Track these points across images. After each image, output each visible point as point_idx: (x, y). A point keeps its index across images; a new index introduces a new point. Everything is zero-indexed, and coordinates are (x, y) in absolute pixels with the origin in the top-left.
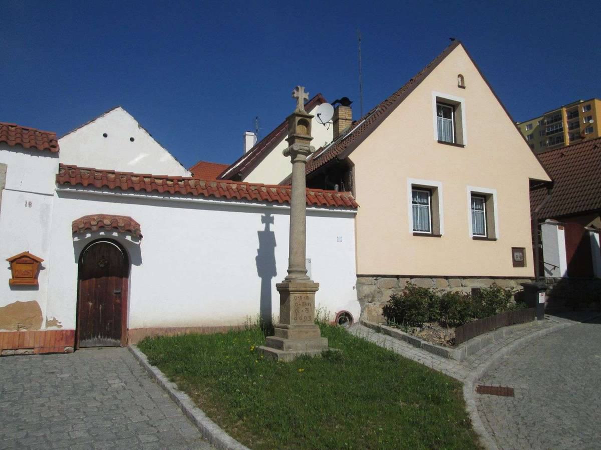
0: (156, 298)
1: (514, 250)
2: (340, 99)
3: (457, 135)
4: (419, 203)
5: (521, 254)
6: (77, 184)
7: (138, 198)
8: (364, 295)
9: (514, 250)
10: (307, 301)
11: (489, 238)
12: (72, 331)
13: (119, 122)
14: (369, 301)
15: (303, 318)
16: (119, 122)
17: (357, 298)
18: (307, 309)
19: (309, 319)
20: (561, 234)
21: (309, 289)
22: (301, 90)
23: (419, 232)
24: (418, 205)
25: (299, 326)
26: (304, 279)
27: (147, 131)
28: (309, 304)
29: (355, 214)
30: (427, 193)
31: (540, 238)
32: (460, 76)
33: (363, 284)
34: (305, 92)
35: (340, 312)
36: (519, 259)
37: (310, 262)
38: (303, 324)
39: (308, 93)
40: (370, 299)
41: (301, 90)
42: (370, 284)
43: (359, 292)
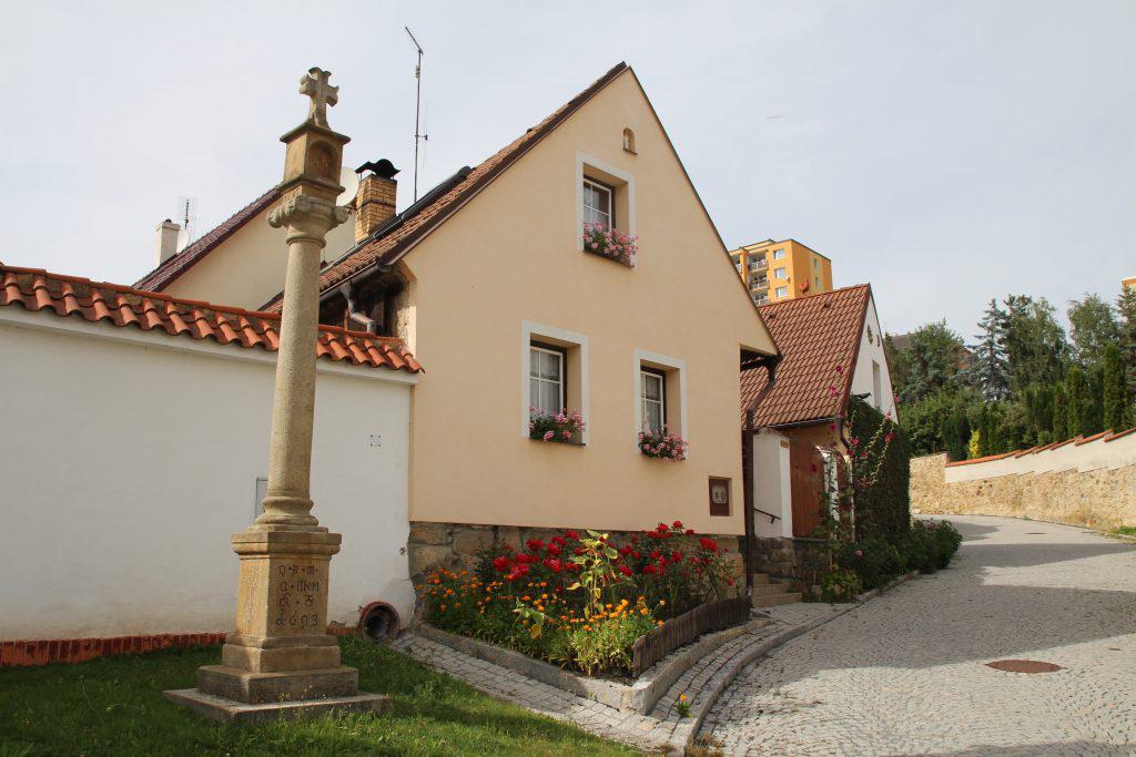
1: (714, 482)
2: (374, 161)
3: (690, 189)
5: (724, 489)
8: (424, 568)
9: (714, 482)
10: (310, 579)
12: (739, 537)
17: (406, 575)
18: (309, 599)
19: (311, 622)
20: (784, 455)
25: (290, 640)
26: (306, 524)
30: (558, 357)
31: (745, 471)
32: (628, 132)
33: (423, 542)
35: (369, 606)
36: (718, 500)
37: (530, 130)
38: (299, 635)
42: (438, 541)
43: (412, 559)
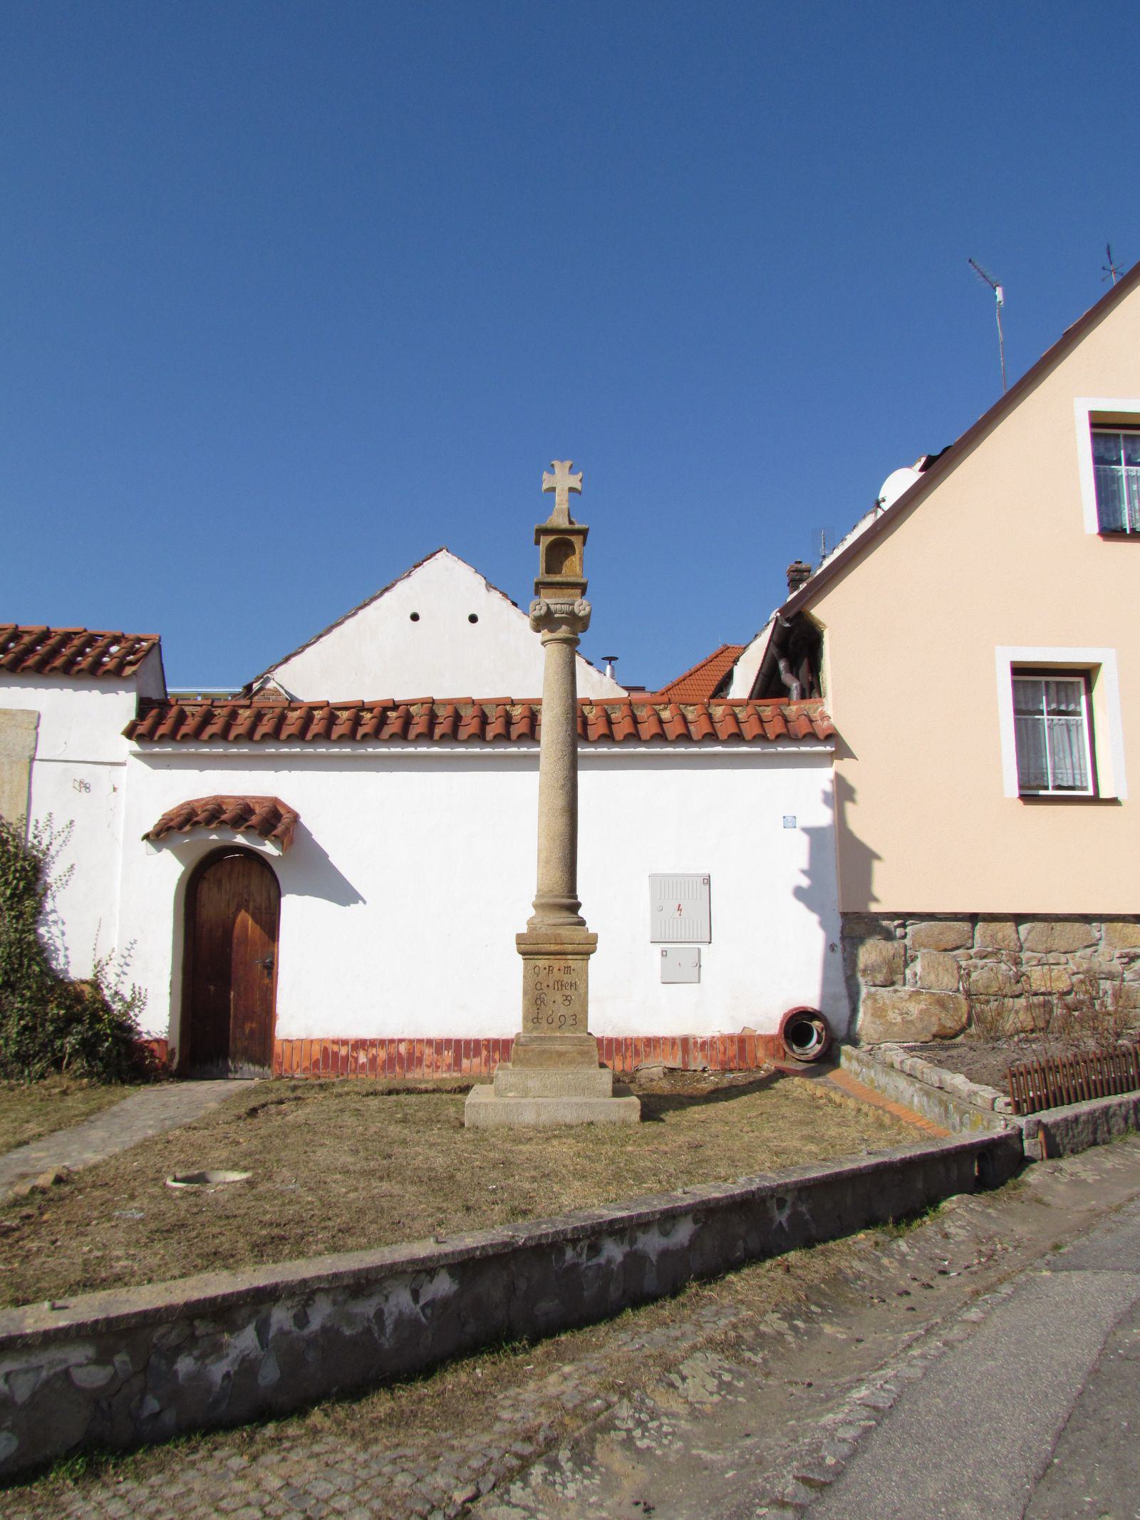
0: (325, 983)
4: (1049, 713)
6: (678, 737)
7: (667, 755)
10: (567, 978)
11: (1103, 795)
13: (446, 583)
14: (877, 982)
15: (556, 1020)
16: (446, 583)
18: (567, 998)
19: (571, 1022)
21: (569, 948)
22: (561, 468)
23: (1051, 792)
24: (1045, 717)
25: (541, 1039)
27: (505, 595)
28: (573, 985)
29: (536, 757)
34: (572, 470)
39: (581, 474)
40: (880, 978)
41: (561, 468)
